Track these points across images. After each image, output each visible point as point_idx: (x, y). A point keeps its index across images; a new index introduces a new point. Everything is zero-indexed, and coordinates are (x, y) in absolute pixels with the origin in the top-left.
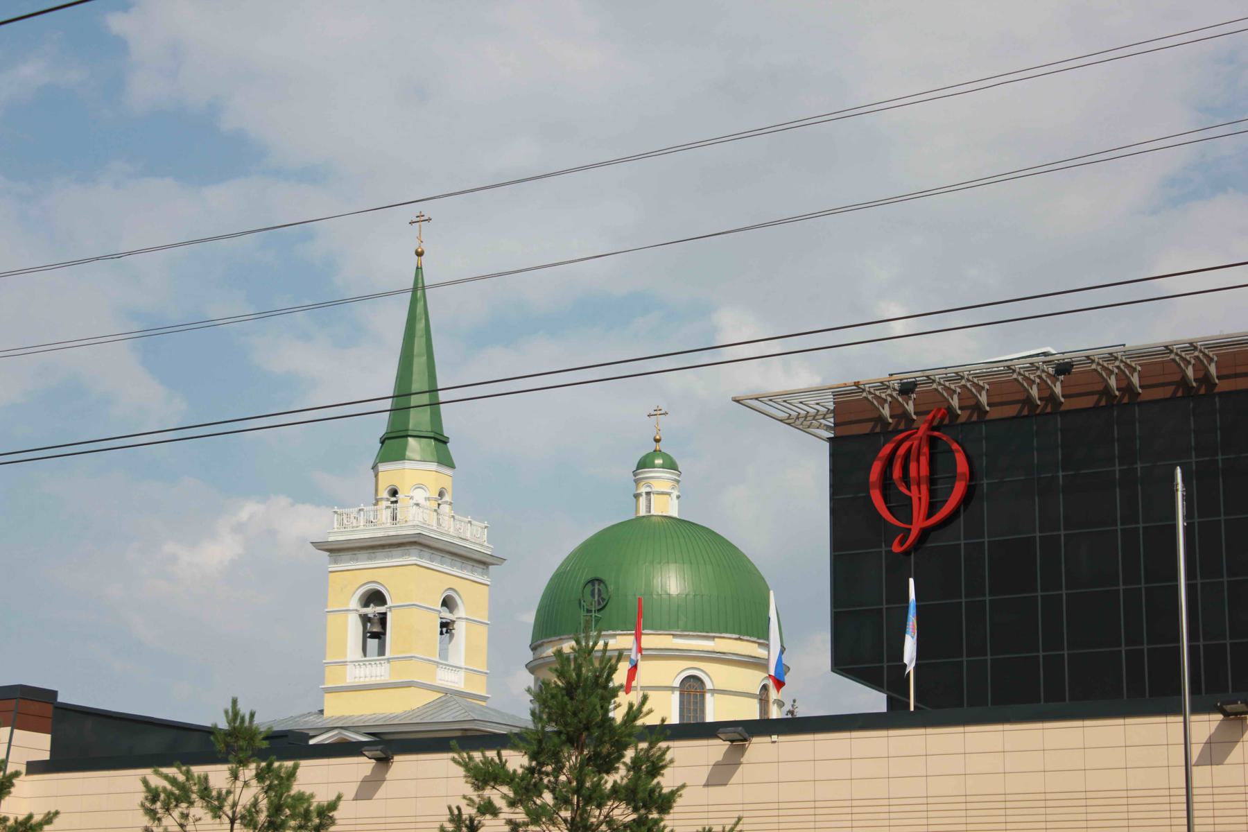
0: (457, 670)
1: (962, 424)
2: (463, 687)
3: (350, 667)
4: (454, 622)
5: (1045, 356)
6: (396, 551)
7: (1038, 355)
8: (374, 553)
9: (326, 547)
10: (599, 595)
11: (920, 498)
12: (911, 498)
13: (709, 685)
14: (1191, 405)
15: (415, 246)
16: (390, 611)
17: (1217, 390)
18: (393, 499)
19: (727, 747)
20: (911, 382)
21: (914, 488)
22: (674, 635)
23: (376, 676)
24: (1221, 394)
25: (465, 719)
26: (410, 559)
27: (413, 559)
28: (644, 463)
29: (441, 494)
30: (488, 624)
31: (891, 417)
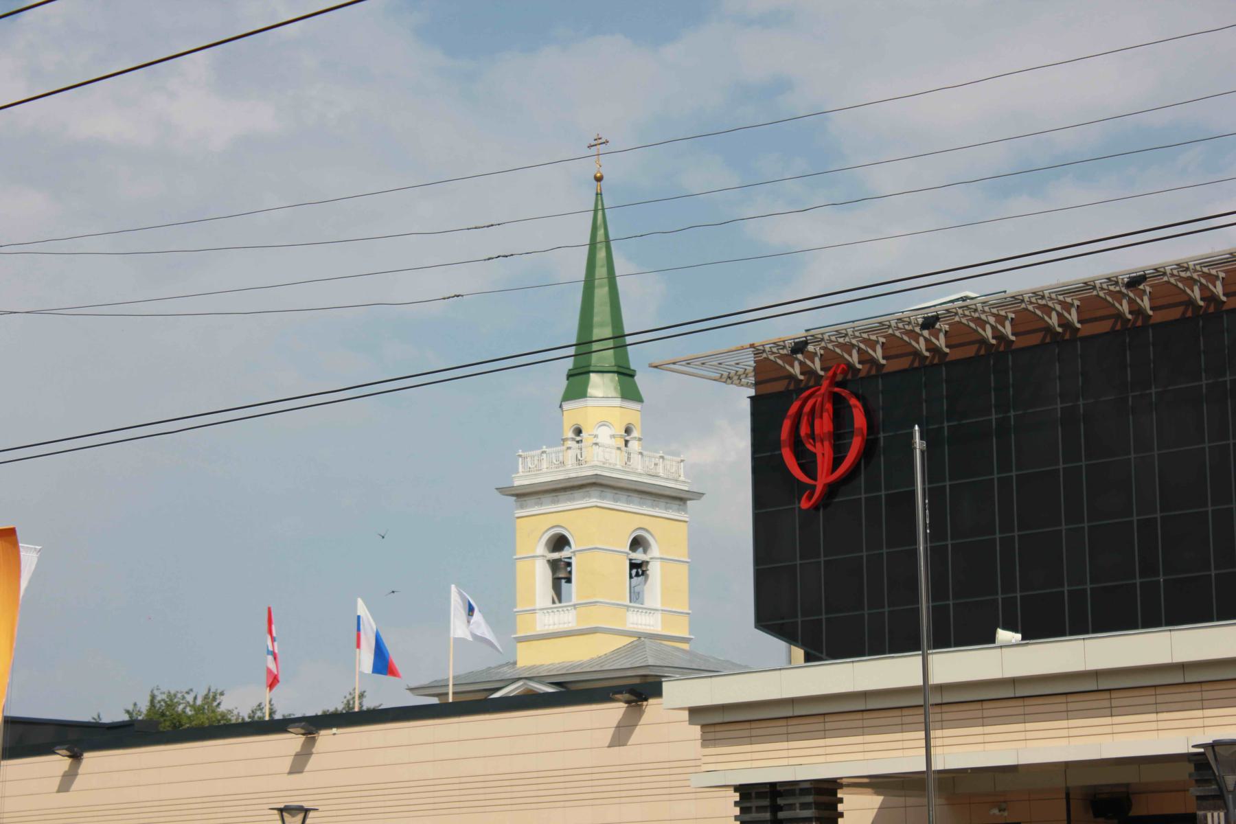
0: (652, 612)
1: (862, 378)
2: (660, 629)
3: (539, 615)
4: (647, 562)
5: (964, 300)
6: (577, 494)
7: (957, 300)
8: (556, 496)
9: (513, 492)
11: (823, 454)
12: (815, 454)
14: (1057, 351)
15: (594, 170)
16: (575, 555)
17: (1079, 335)
18: (578, 438)
19: (623, 711)
20: (802, 341)
21: (818, 445)
23: (549, 625)
24: (1154, 326)
25: (549, 674)
26: (591, 500)
29: (628, 431)
30: (687, 562)
31: (1059, 326)
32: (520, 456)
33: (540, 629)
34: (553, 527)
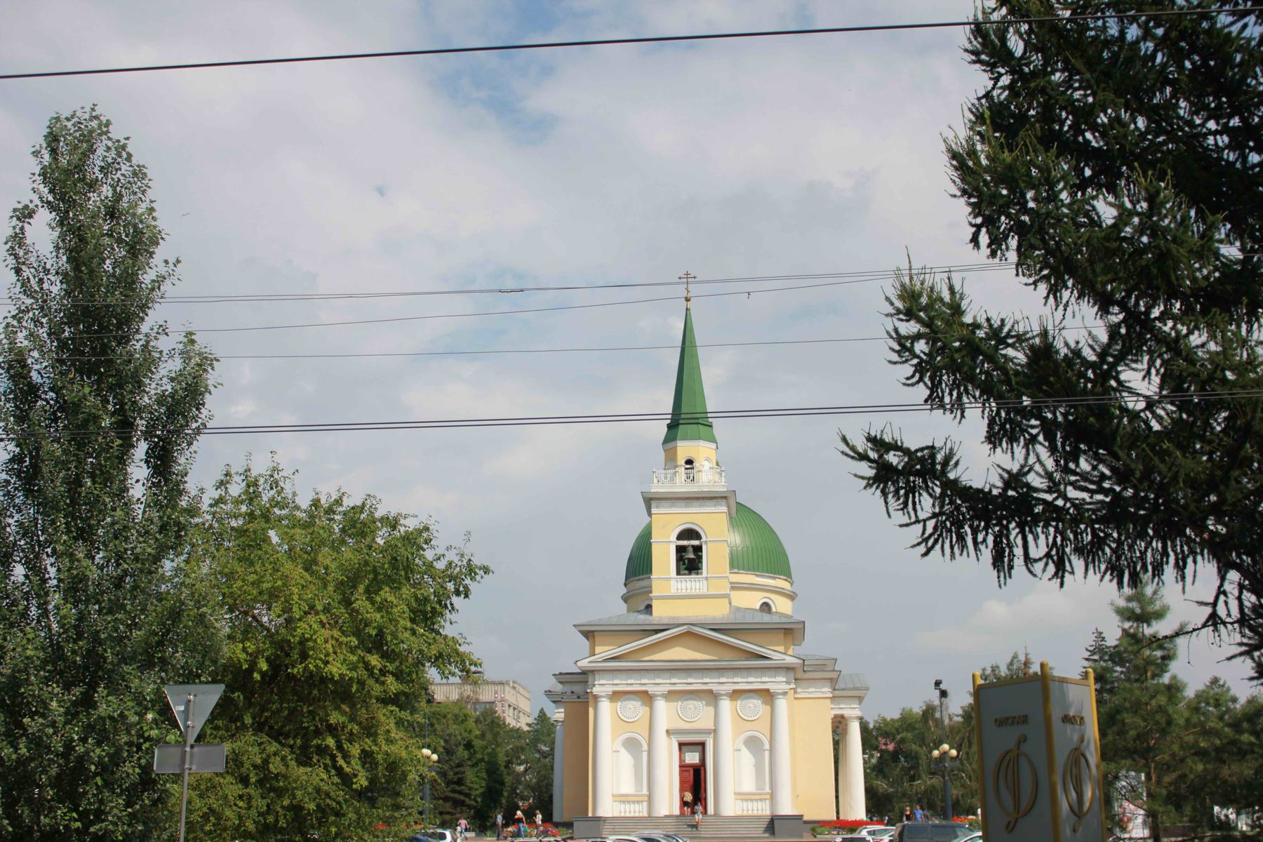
33: (673, 591)
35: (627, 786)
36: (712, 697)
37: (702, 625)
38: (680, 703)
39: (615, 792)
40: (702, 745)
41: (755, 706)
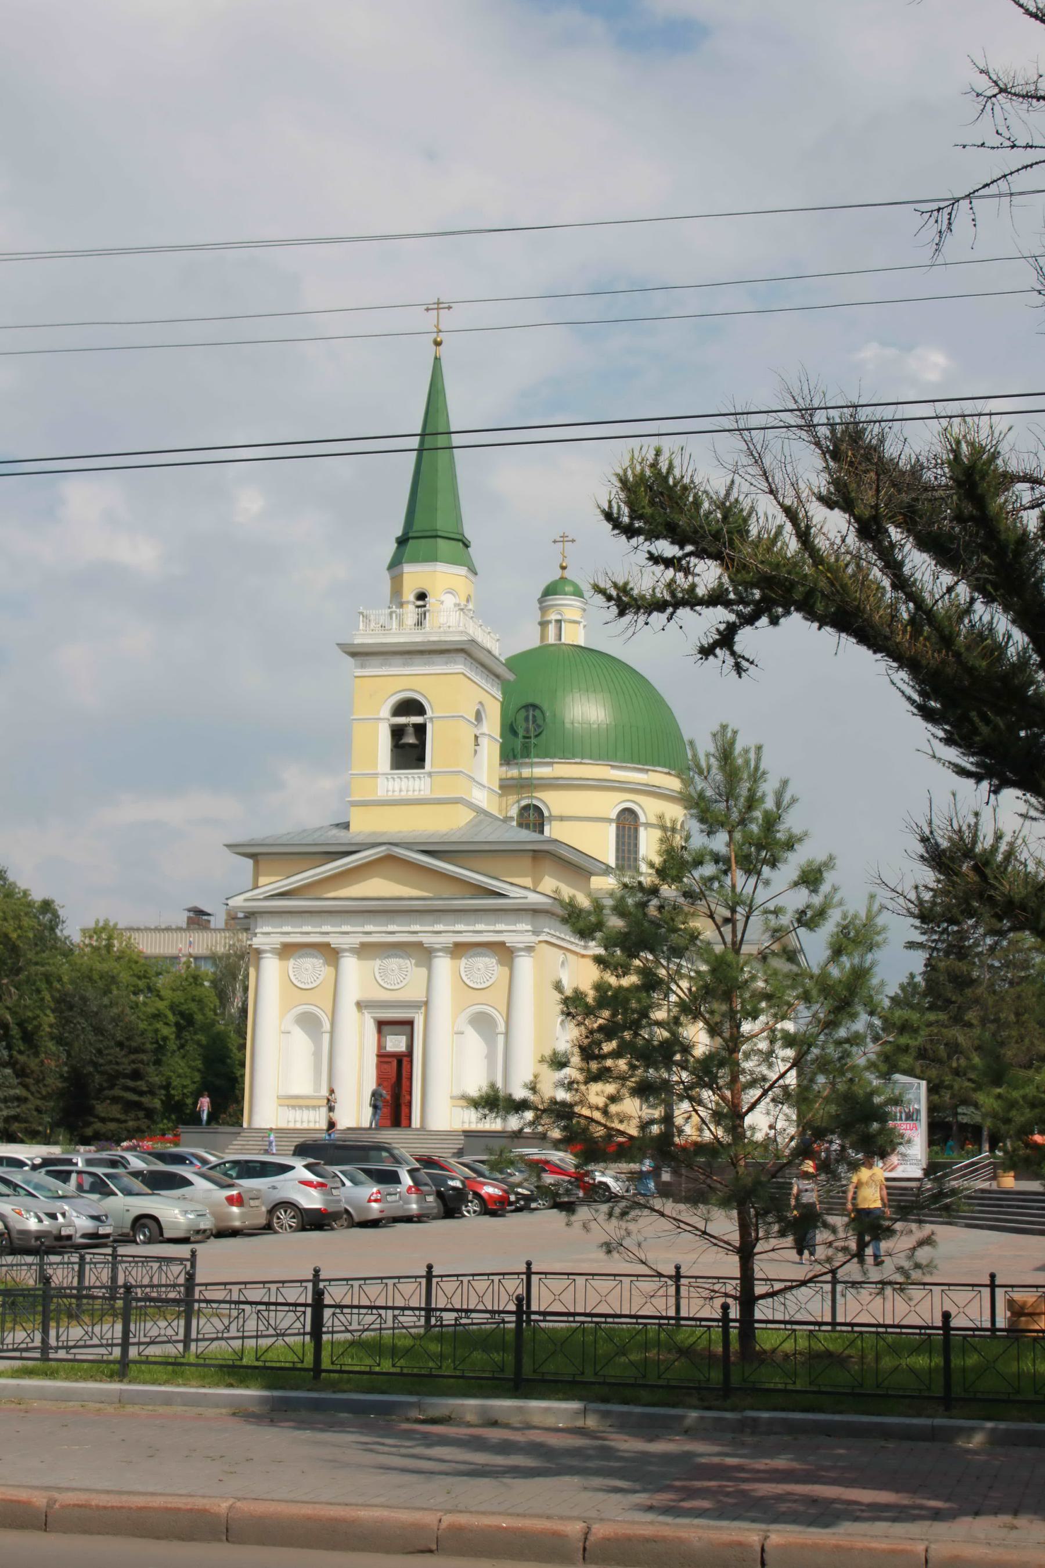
10: (534, 722)
13: (642, 819)
22: (612, 767)
27: (459, 668)
28: (551, 591)
32: (362, 613)
33: (381, 794)
34: (400, 691)
35: (302, 1084)
36: (423, 953)
37: (408, 846)
38: (378, 962)
39: (282, 1093)
40: (410, 1023)
41: (486, 965)
